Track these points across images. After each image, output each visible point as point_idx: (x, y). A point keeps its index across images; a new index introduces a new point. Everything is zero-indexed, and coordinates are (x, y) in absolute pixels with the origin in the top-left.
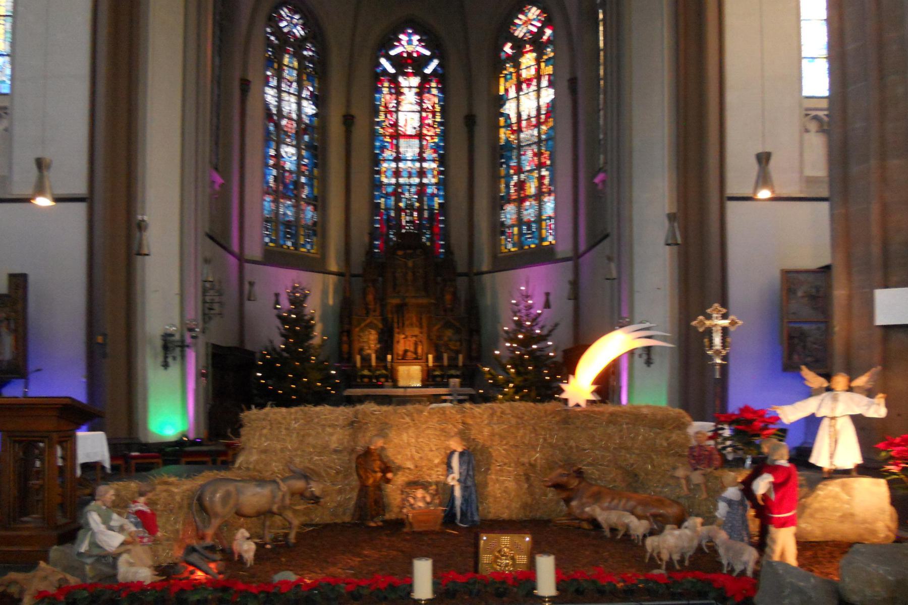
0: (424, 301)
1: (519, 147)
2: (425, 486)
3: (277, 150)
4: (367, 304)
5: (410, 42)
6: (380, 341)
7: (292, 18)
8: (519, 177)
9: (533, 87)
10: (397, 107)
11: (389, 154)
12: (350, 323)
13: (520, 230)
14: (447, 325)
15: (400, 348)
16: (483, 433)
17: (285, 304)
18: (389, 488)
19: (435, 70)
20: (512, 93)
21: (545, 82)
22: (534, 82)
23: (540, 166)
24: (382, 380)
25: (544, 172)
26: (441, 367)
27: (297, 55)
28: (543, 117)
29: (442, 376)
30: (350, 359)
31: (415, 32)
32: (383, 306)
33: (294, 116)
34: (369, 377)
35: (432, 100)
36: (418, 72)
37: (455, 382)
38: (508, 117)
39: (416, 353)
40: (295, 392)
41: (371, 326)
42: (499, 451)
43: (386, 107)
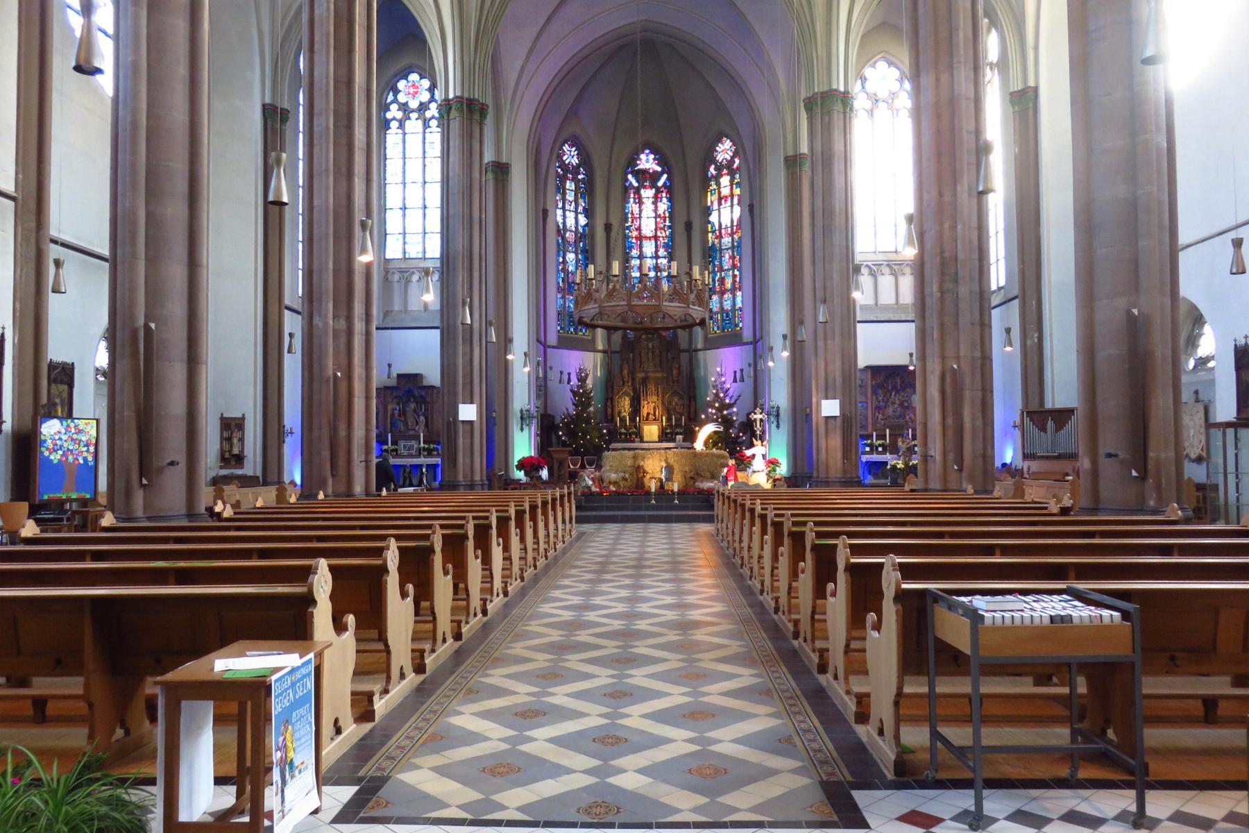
0: (659, 375)
1: (721, 250)
2: (655, 478)
3: (564, 257)
4: (623, 378)
5: (647, 161)
6: (632, 405)
7: (571, 151)
8: (721, 275)
9: (729, 203)
10: (640, 214)
11: (635, 253)
12: (612, 392)
13: (722, 316)
14: (675, 393)
15: (645, 411)
16: (671, 461)
17: (574, 381)
18: (645, 479)
19: (665, 183)
20: (716, 206)
21: (736, 200)
22: (729, 200)
23: (734, 267)
24: (634, 436)
25: (737, 273)
26: (671, 426)
27: (574, 179)
28: (735, 228)
29: (671, 433)
30: (612, 420)
31: (651, 152)
32: (633, 379)
33: (573, 229)
34: (626, 434)
35: (663, 206)
36: (653, 185)
37: (679, 437)
38: (713, 225)
39: (655, 415)
40: (582, 446)
41: (626, 394)
42: (676, 467)
43: (632, 214)
